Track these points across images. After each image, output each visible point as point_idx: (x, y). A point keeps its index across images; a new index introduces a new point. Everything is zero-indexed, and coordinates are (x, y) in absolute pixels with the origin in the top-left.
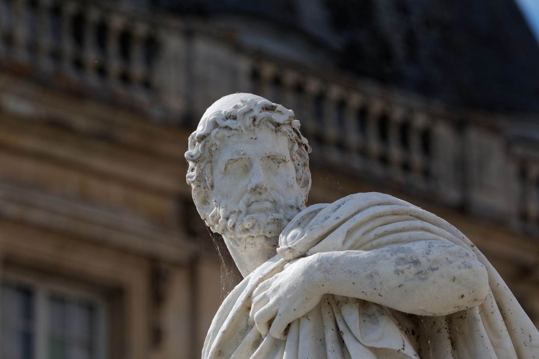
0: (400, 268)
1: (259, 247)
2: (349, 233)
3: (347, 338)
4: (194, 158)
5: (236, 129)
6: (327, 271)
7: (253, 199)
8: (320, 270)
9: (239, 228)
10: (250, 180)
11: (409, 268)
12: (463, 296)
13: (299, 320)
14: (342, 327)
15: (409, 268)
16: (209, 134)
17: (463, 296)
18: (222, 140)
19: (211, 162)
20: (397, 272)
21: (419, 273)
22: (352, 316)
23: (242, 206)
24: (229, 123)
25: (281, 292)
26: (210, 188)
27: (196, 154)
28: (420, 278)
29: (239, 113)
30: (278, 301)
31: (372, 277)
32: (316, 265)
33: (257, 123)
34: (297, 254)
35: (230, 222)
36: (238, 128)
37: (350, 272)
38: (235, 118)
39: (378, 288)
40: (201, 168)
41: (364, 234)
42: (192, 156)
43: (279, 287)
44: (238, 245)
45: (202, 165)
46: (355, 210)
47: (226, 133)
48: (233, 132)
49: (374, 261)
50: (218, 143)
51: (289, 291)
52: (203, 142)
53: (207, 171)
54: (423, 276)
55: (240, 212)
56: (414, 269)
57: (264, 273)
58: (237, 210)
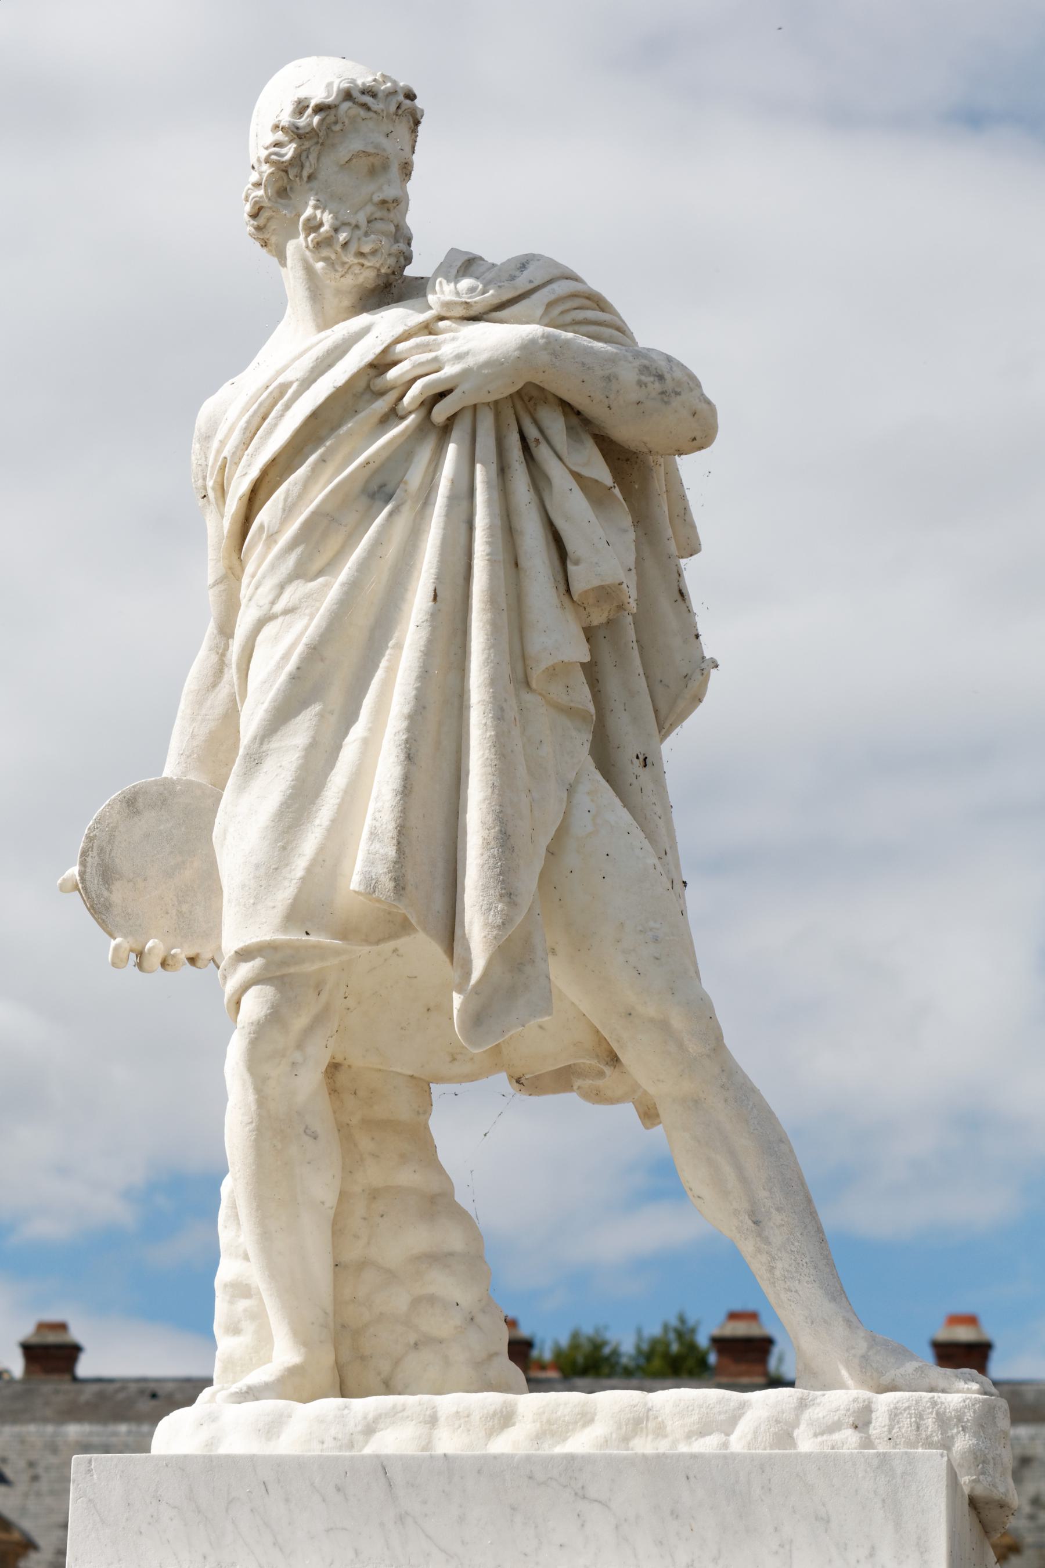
0: (643, 378)
1: (361, 279)
2: (550, 305)
3: (543, 453)
4: (301, 131)
5: (375, 112)
6: (554, 354)
7: (378, 215)
8: (546, 349)
9: (353, 248)
10: (380, 189)
11: (653, 383)
12: (694, 439)
13: (475, 407)
14: (532, 432)
15: (653, 383)
16: (336, 106)
17: (694, 439)
18: (353, 120)
19: (322, 144)
20: (640, 384)
21: (663, 393)
22: (556, 425)
23: (361, 218)
24: (367, 99)
25: (470, 362)
26: (305, 179)
27: (304, 127)
28: (663, 400)
29: (383, 91)
30: (465, 373)
31: (610, 380)
32: (542, 341)
33: (400, 112)
34: (472, 313)
35: (343, 236)
36: (379, 111)
37: (583, 364)
38: (374, 95)
39: (612, 397)
40: (303, 147)
41: (562, 313)
42: (298, 128)
43: (467, 353)
44: (336, 271)
45: (307, 144)
46: (547, 278)
47: (362, 113)
48: (371, 114)
49: (613, 359)
50: (347, 122)
51: (487, 364)
52: (322, 115)
53: (313, 157)
54: (666, 399)
55: (357, 227)
56: (657, 386)
57: (409, 324)
58: (354, 222)
